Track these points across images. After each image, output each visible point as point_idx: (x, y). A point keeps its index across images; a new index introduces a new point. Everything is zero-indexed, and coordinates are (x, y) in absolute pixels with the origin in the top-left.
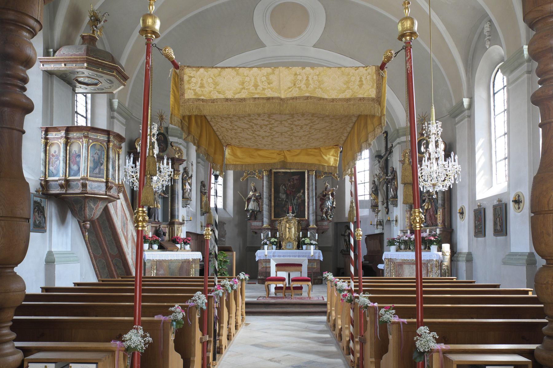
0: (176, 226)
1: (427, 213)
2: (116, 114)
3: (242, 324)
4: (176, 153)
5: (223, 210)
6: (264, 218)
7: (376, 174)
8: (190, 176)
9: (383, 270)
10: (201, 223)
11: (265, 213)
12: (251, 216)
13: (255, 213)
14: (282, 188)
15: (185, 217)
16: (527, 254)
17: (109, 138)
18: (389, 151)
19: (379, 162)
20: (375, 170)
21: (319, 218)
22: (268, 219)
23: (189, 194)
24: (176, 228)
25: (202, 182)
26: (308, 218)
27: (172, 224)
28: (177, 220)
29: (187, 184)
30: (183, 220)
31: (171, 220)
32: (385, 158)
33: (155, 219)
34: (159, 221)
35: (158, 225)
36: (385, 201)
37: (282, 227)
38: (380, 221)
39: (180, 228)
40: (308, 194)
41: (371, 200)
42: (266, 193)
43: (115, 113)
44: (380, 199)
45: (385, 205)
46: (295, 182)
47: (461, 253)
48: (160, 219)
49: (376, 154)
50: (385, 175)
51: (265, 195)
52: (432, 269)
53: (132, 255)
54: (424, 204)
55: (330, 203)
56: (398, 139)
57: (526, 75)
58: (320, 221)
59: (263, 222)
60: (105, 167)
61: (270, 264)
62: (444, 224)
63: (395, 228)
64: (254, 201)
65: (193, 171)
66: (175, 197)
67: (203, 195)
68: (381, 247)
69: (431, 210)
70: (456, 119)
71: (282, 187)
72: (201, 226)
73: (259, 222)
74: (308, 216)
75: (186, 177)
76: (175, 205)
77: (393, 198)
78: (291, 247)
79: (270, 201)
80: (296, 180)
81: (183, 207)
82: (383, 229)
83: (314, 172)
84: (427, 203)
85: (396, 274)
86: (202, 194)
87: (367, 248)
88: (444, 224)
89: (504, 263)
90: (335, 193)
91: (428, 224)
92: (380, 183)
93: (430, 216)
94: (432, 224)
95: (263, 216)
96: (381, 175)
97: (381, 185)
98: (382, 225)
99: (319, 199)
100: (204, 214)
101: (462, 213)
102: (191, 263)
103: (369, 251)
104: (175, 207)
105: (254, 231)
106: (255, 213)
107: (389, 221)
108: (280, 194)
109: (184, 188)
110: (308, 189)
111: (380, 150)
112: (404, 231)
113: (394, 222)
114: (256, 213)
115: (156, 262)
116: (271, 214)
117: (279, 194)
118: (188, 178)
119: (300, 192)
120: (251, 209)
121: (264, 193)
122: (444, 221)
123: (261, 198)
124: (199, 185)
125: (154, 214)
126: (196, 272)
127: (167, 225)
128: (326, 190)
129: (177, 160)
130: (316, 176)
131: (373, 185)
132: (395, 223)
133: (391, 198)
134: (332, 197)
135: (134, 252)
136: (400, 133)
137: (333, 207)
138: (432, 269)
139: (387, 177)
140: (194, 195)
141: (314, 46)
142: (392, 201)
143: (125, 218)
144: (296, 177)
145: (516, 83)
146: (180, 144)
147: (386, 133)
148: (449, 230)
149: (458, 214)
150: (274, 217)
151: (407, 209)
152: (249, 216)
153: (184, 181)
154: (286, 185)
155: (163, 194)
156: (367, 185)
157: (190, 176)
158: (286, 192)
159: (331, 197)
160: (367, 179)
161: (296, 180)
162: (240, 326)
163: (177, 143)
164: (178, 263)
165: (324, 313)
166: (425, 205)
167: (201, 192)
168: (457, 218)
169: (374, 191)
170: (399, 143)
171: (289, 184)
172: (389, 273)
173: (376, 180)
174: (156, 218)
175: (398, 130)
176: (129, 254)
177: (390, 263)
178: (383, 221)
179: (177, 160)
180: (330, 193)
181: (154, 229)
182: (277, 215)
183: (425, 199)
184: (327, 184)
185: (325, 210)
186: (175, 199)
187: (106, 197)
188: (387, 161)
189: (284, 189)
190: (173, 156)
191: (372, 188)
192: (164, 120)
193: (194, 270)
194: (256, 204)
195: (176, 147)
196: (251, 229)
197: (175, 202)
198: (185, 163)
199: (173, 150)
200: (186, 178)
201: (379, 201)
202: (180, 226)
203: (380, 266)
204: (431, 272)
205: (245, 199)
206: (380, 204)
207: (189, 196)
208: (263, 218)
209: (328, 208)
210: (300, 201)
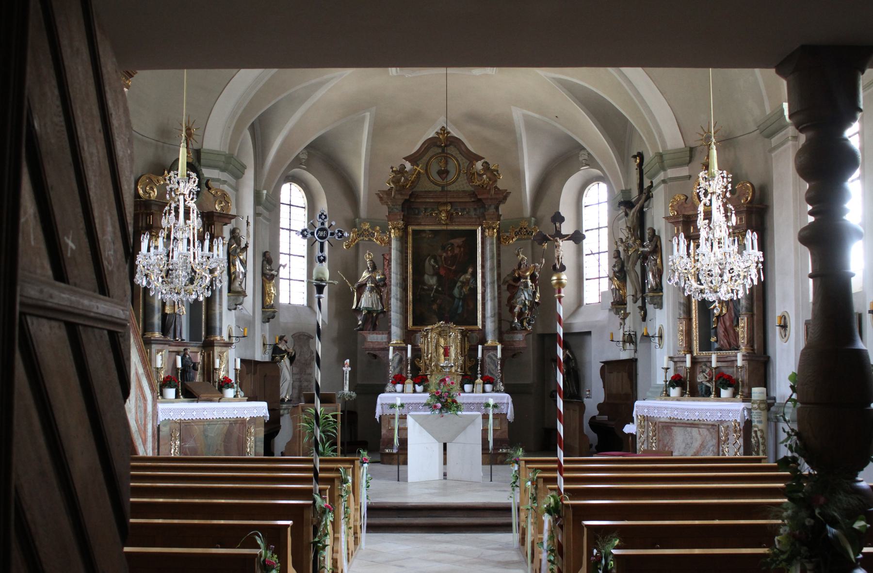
0: (217, 350)
1: (719, 324)
3: (355, 550)
4: (217, 202)
5: (308, 309)
6: (392, 326)
7: (621, 239)
8: (243, 245)
9: (633, 436)
10: (264, 337)
11: (395, 316)
12: (365, 321)
13: (375, 315)
14: (429, 263)
15: (233, 329)
18: (646, 194)
19: (627, 215)
20: (620, 231)
21: (506, 327)
22: (401, 328)
23: (241, 282)
24: (216, 354)
25: (265, 254)
26: (484, 326)
27: (208, 346)
28: (218, 338)
29: (237, 263)
30: (230, 337)
31: (206, 338)
32: (638, 206)
33: (175, 337)
35: (182, 349)
36: (639, 295)
37: (430, 345)
38: (630, 334)
40: (483, 277)
41: (612, 290)
42: (397, 274)
44: (630, 290)
45: (639, 303)
48: (185, 335)
50: (638, 242)
52: (727, 435)
53: (137, 413)
55: (529, 295)
56: (662, 173)
58: (508, 332)
59: (389, 333)
61: (406, 422)
62: (752, 346)
63: (658, 350)
64: (372, 290)
65: (247, 236)
67: (268, 281)
68: (632, 388)
69: (727, 317)
71: (429, 261)
72: (264, 345)
73: (383, 334)
74: (484, 322)
75: (236, 249)
76: (215, 306)
77: (653, 290)
79: (405, 289)
81: (230, 310)
82: (636, 351)
83: (495, 230)
85: (659, 445)
86: (265, 279)
87: (604, 387)
88: (752, 346)
90: (539, 273)
92: (629, 257)
93: (726, 329)
94: (730, 344)
95: (390, 322)
96: (631, 242)
97: (630, 263)
99: (506, 286)
100: (269, 319)
101: (784, 327)
102: (247, 425)
103: (608, 395)
104: (214, 310)
105: (372, 352)
107: (647, 337)
108: (426, 277)
110: (483, 267)
111: (629, 188)
113: (657, 338)
114: (377, 316)
115: (180, 423)
117: (423, 275)
118: (238, 250)
119: (466, 272)
120: (366, 308)
121: (393, 276)
122: (751, 341)
123: (385, 285)
124: (260, 260)
125: (173, 326)
126: (258, 443)
127: (199, 347)
128: (519, 268)
129: (219, 217)
130: (498, 238)
131: (615, 260)
132: (657, 341)
133: (650, 292)
134: (532, 282)
135: (139, 407)
137: (533, 303)
138: (727, 435)
140: (250, 284)
142: (652, 297)
144: (458, 241)
146: (225, 182)
147: (641, 155)
148: (762, 359)
149: (778, 328)
151: (680, 314)
152: (360, 322)
153: (231, 257)
154: (438, 258)
156: (605, 259)
157: (243, 245)
158: (436, 273)
159: (530, 283)
160: (605, 245)
162: (352, 555)
163: (218, 180)
164: (222, 426)
167: (264, 274)
169: (617, 272)
170: (664, 181)
171: (444, 254)
172: (645, 443)
173: (621, 249)
175: (661, 156)
176: (130, 412)
177: (648, 424)
178: (635, 335)
179: (219, 217)
180: (528, 273)
182: (420, 320)
184: (521, 256)
185: (517, 310)
188: (641, 217)
189: (433, 266)
190: (211, 209)
191: (614, 266)
192: (194, 136)
193: (253, 438)
194: (375, 296)
195: (217, 191)
196: (366, 349)
198: (233, 221)
199: (211, 196)
200: (236, 250)
201: (628, 294)
202: (224, 349)
203: (629, 429)
204: (725, 442)
205: (353, 285)
206: (629, 300)
207: (242, 288)
208: (390, 327)
209: (525, 305)
210: (465, 290)
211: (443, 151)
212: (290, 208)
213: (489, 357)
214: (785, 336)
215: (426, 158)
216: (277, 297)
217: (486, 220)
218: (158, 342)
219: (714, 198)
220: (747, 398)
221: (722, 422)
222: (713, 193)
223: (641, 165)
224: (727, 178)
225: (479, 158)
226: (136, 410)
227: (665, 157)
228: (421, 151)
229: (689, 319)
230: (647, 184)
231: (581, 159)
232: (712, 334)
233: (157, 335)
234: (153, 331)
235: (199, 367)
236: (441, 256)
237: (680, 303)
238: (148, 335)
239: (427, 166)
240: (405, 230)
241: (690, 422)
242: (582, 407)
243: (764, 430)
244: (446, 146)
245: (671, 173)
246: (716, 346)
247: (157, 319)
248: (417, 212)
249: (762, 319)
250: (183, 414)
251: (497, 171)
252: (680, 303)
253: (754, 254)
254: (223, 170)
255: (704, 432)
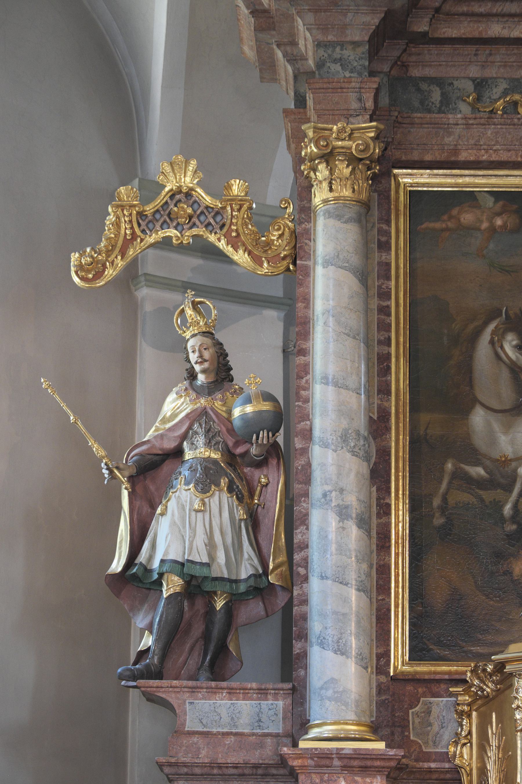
13: (220, 604)
106: (220, 604)
248: (436, 96)
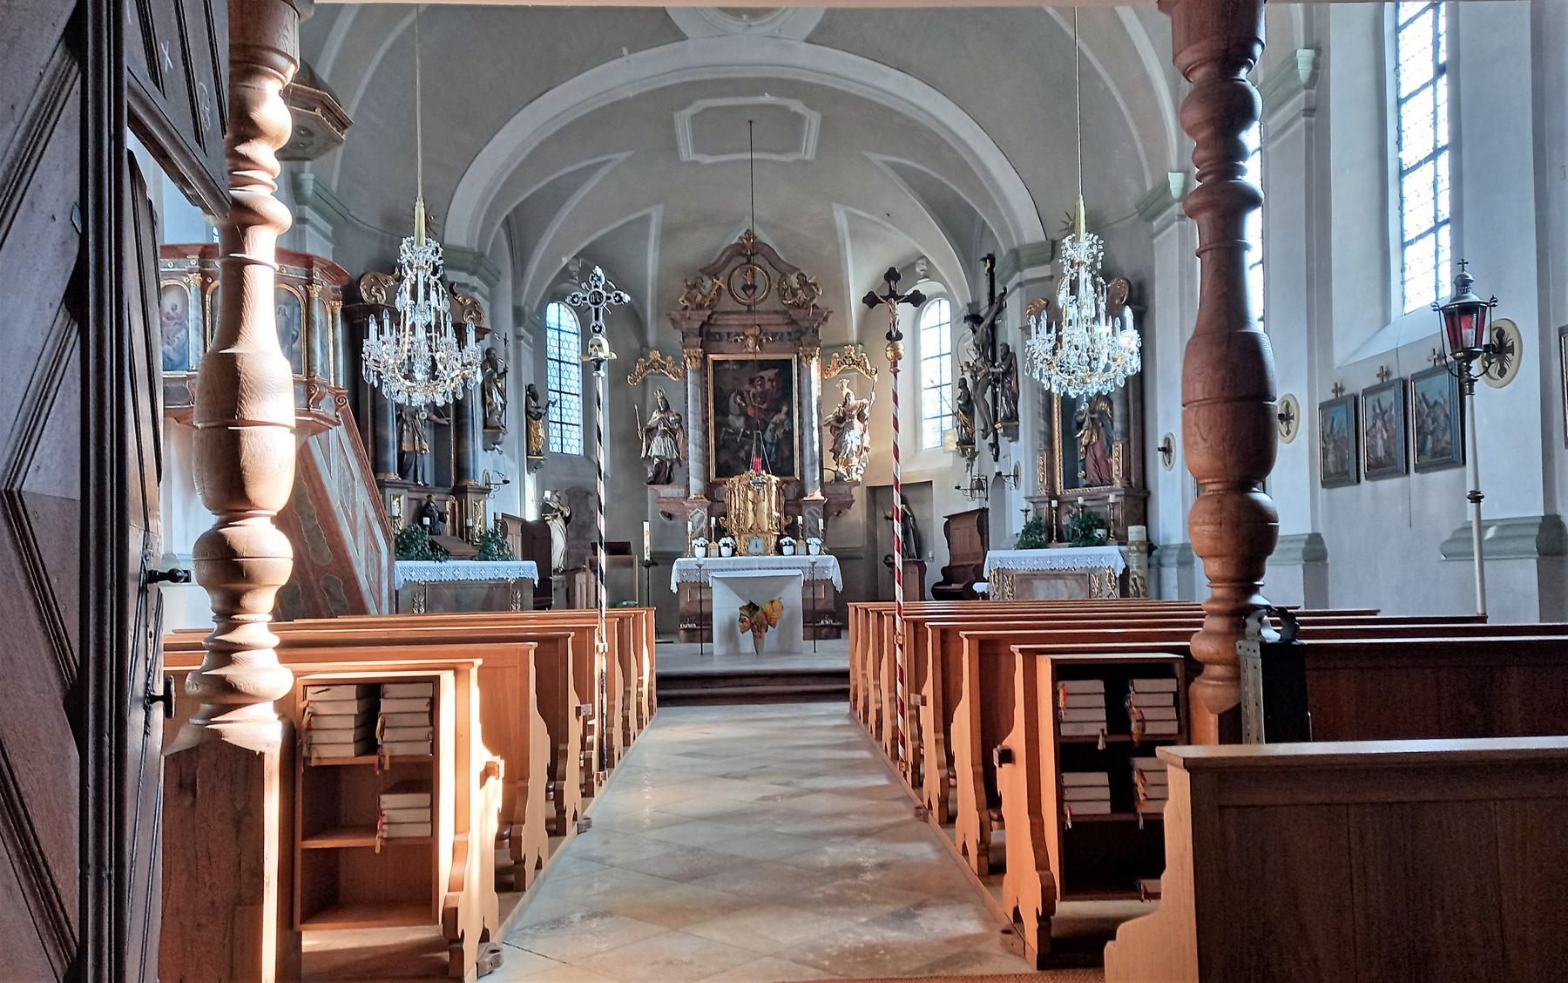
0: (471, 497)
1: (1088, 454)
2: (308, 212)
8: (501, 370)
11: (694, 465)
14: (734, 402)
16: (1306, 537)
17: (309, 274)
18: (997, 302)
19: (974, 332)
25: (529, 388)
26: (802, 476)
27: (460, 491)
28: (472, 483)
31: (456, 482)
32: (987, 322)
33: (416, 480)
34: (425, 485)
35: (425, 496)
39: (481, 502)
43: (306, 207)
44: (978, 424)
45: (990, 439)
46: (768, 385)
47: (1166, 547)
49: (966, 312)
50: (989, 364)
51: (692, 420)
54: (1082, 432)
56: (1018, 274)
57: (1303, 120)
59: (688, 487)
60: (304, 347)
62: (1129, 479)
66: (467, 424)
69: (1098, 446)
70: (1155, 224)
75: (491, 374)
77: (1006, 419)
78: (760, 549)
79: (706, 433)
80: (769, 380)
84: (1088, 429)
88: (1129, 479)
89: (687, 38)
91: (1092, 482)
92: (976, 384)
93: (1096, 462)
96: (979, 364)
98: (983, 489)
101: (1166, 450)
108: (731, 417)
109: (488, 402)
112: (1036, 500)
116: (708, 469)
135: (371, 559)
136: (1024, 260)
139: (992, 370)
140: (513, 420)
141: (808, 40)
143: (347, 474)
144: (769, 374)
145: (1282, 138)
147: (991, 258)
148: (1141, 494)
150: (718, 475)
154: (745, 394)
155: (434, 417)
157: (501, 370)
158: (744, 413)
160: (947, 377)
161: (769, 380)
163: (465, 285)
165: (842, 695)
166: (1082, 435)
167: (528, 412)
168: (1156, 460)
170: (1020, 285)
171: (753, 390)
174: (419, 477)
176: (359, 565)
177: (1003, 578)
181: (414, 504)
182: (725, 471)
183: (1084, 420)
186: (467, 429)
187: (310, 419)
197: (467, 436)
202: (481, 496)
206: (977, 436)
209: (851, 451)
210: (779, 433)
211: (749, 262)
212: (559, 325)
213: (809, 513)
214: (1168, 463)
215: (728, 270)
216: (547, 442)
217: (802, 346)
218: (393, 485)
219: (1082, 269)
220: (1122, 540)
221: (1093, 570)
222: (1079, 264)
223: (991, 271)
224: (1097, 245)
225: (793, 269)
226: (367, 562)
227: (1022, 253)
228: (721, 262)
229: (1052, 451)
230: (999, 291)
231: (918, 270)
232: (1080, 468)
233: (394, 476)
234: (387, 472)
235: (448, 517)
236: (748, 392)
237: (1040, 431)
238: (381, 477)
239: (729, 280)
240: (704, 360)
241: (1055, 572)
242: (923, 569)
243: (1145, 576)
244: (752, 255)
245: (1030, 273)
246: (1085, 482)
247: (392, 457)
248: (718, 337)
249: (1141, 466)
250: (428, 573)
251: (815, 285)
252: (1040, 431)
253: (1129, 339)
254: (472, 273)
255: (1071, 583)
